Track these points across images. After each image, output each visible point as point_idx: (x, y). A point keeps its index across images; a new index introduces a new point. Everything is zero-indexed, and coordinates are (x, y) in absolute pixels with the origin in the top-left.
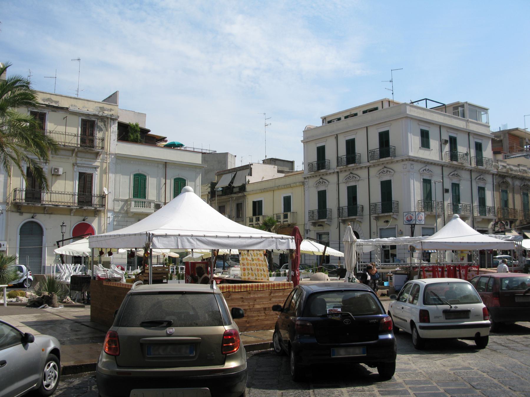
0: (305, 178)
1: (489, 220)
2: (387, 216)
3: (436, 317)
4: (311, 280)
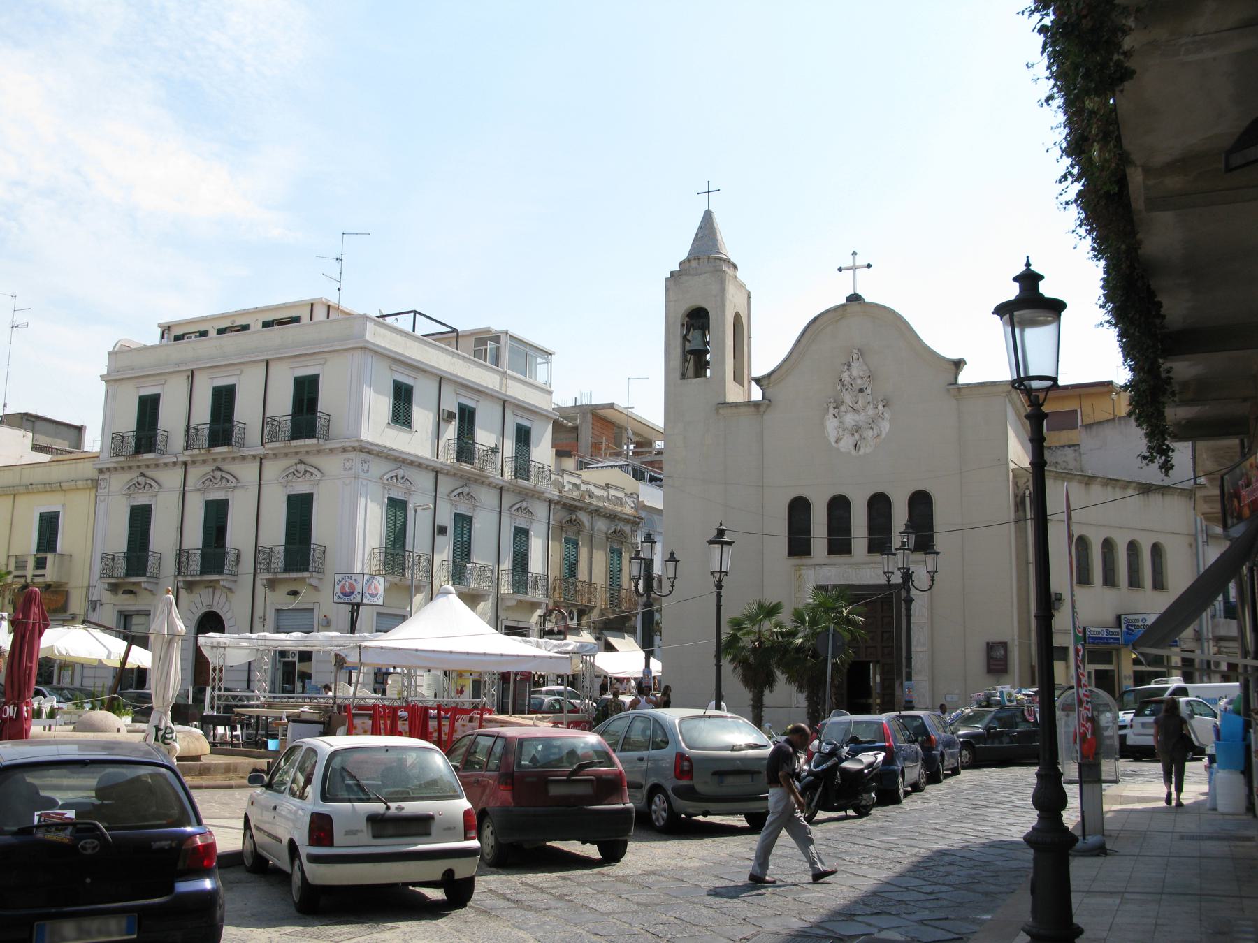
0: (101, 471)
1: (534, 606)
2: (295, 579)
3: (349, 833)
4: (75, 730)
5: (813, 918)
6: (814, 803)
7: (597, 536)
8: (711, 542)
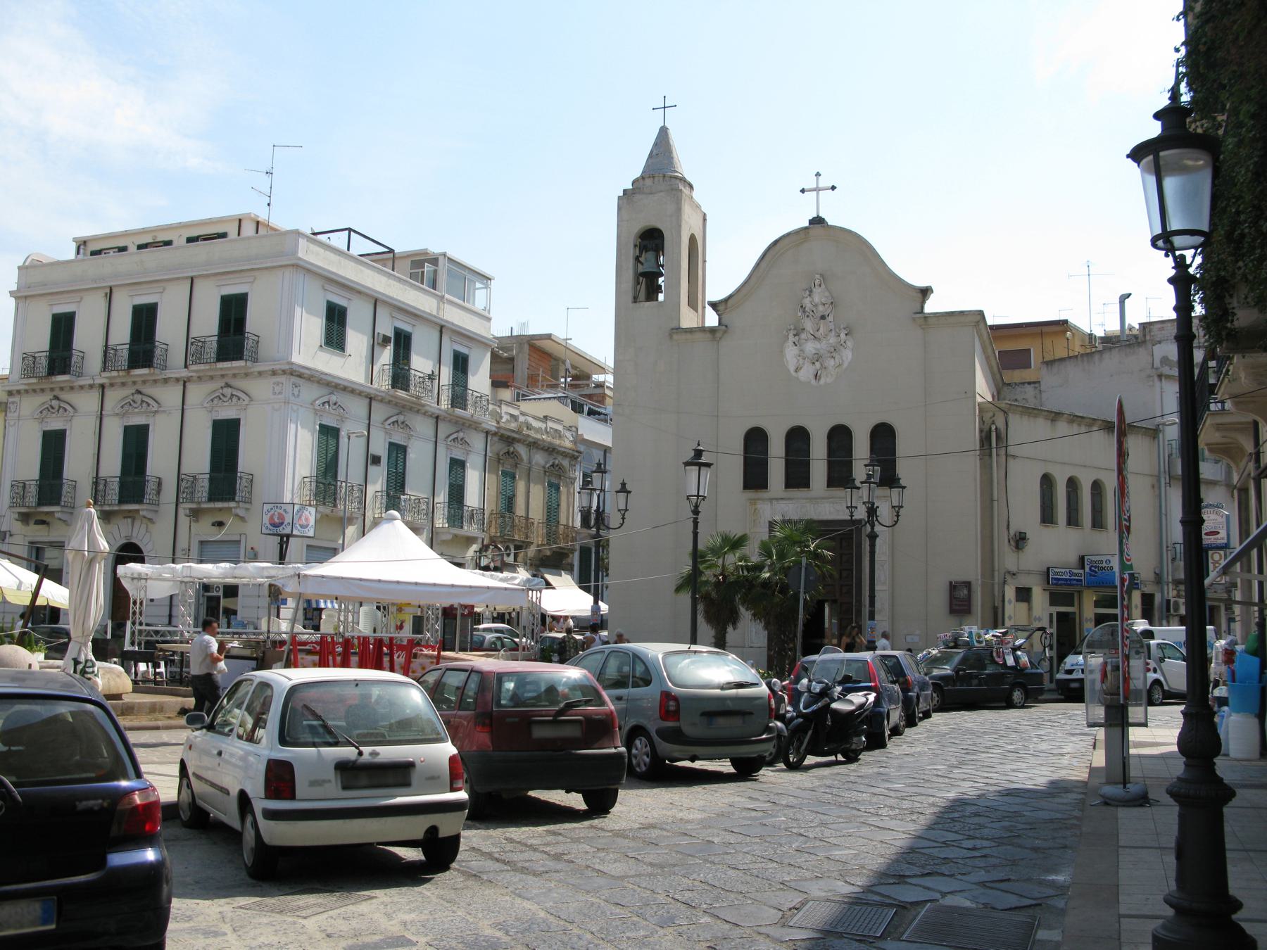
0: (10, 393)
1: (470, 540)
2: (220, 509)
5: (861, 881)
6: (804, 747)
7: (535, 469)
8: (687, 464)
